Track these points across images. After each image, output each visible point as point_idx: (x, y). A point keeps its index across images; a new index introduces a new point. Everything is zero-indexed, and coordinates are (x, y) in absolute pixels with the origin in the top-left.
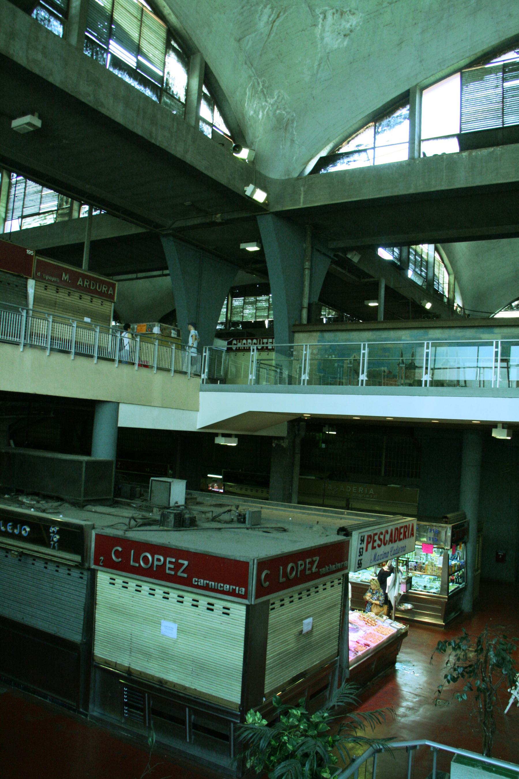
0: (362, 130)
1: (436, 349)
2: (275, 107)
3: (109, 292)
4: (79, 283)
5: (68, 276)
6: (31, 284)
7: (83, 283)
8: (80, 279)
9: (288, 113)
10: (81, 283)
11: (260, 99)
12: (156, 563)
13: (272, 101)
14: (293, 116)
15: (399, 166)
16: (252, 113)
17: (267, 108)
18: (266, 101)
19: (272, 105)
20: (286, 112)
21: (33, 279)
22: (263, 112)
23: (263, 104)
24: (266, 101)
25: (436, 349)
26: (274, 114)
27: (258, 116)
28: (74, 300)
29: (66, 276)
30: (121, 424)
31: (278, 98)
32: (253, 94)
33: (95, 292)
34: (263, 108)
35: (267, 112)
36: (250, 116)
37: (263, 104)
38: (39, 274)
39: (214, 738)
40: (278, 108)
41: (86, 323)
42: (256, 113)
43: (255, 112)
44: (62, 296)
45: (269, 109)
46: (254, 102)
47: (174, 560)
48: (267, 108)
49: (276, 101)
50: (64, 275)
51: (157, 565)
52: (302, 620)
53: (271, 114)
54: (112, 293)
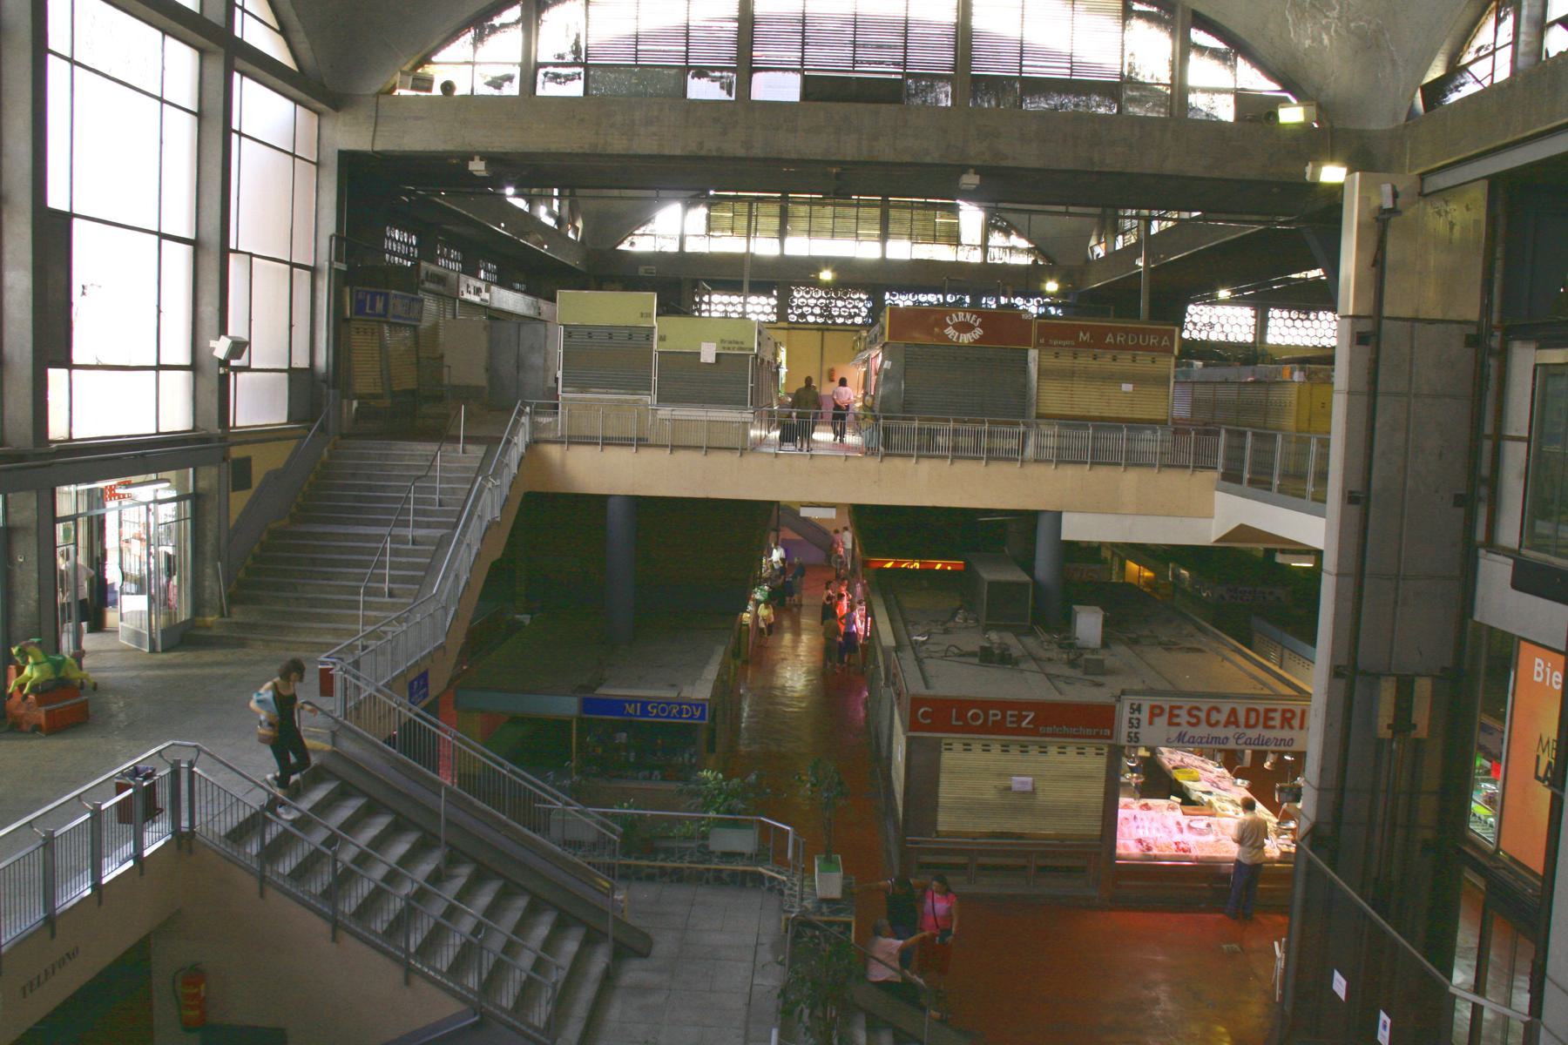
0: (1484, 18)
1: (77, 510)
2: (1344, 19)
3: (1163, 343)
4: (1108, 340)
5: (1088, 335)
6: (1033, 354)
7: (1115, 339)
8: (1110, 335)
9: (1369, 23)
10: (1112, 341)
11: (1315, 17)
12: (991, 718)
13: (1335, 14)
14: (1378, 24)
15: (676, 253)
16: (1308, 43)
17: (1333, 25)
18: (1327, 17)
19: (1339, 18)
20: (1366, 21)
21: (1034, 348)
22: (1328, 33)
23: (1324, 22)
24: (1327, 17)
25: (77, 510)
26: (1349, 31)
27: (1321, 41)
28: (1105, 362)
29: (1085, 334)
30: (1065, 537)
31: (1341, 7)
32: (1299, 16)
33: (1137, 347)
34: (1327, 28)
35: (1336, 31)
36: (1305, 49)
37: (1324, 22)
38: (1042, 341)
39: (168, 799)
40: (1349, 21)
41: (1126, 393)
42: (1317, 39)
43: (1313, 40)
44: (1084, 361)
45: (1337, 25)
46: (1305, 25)
47: (1016, 713)
48: (1333, 25)
49: (1340, 12)
50: (1081, 334)
51: (993, 721)
52: (1013, 775)
53: (1344, 33)
54: (1168, 343)
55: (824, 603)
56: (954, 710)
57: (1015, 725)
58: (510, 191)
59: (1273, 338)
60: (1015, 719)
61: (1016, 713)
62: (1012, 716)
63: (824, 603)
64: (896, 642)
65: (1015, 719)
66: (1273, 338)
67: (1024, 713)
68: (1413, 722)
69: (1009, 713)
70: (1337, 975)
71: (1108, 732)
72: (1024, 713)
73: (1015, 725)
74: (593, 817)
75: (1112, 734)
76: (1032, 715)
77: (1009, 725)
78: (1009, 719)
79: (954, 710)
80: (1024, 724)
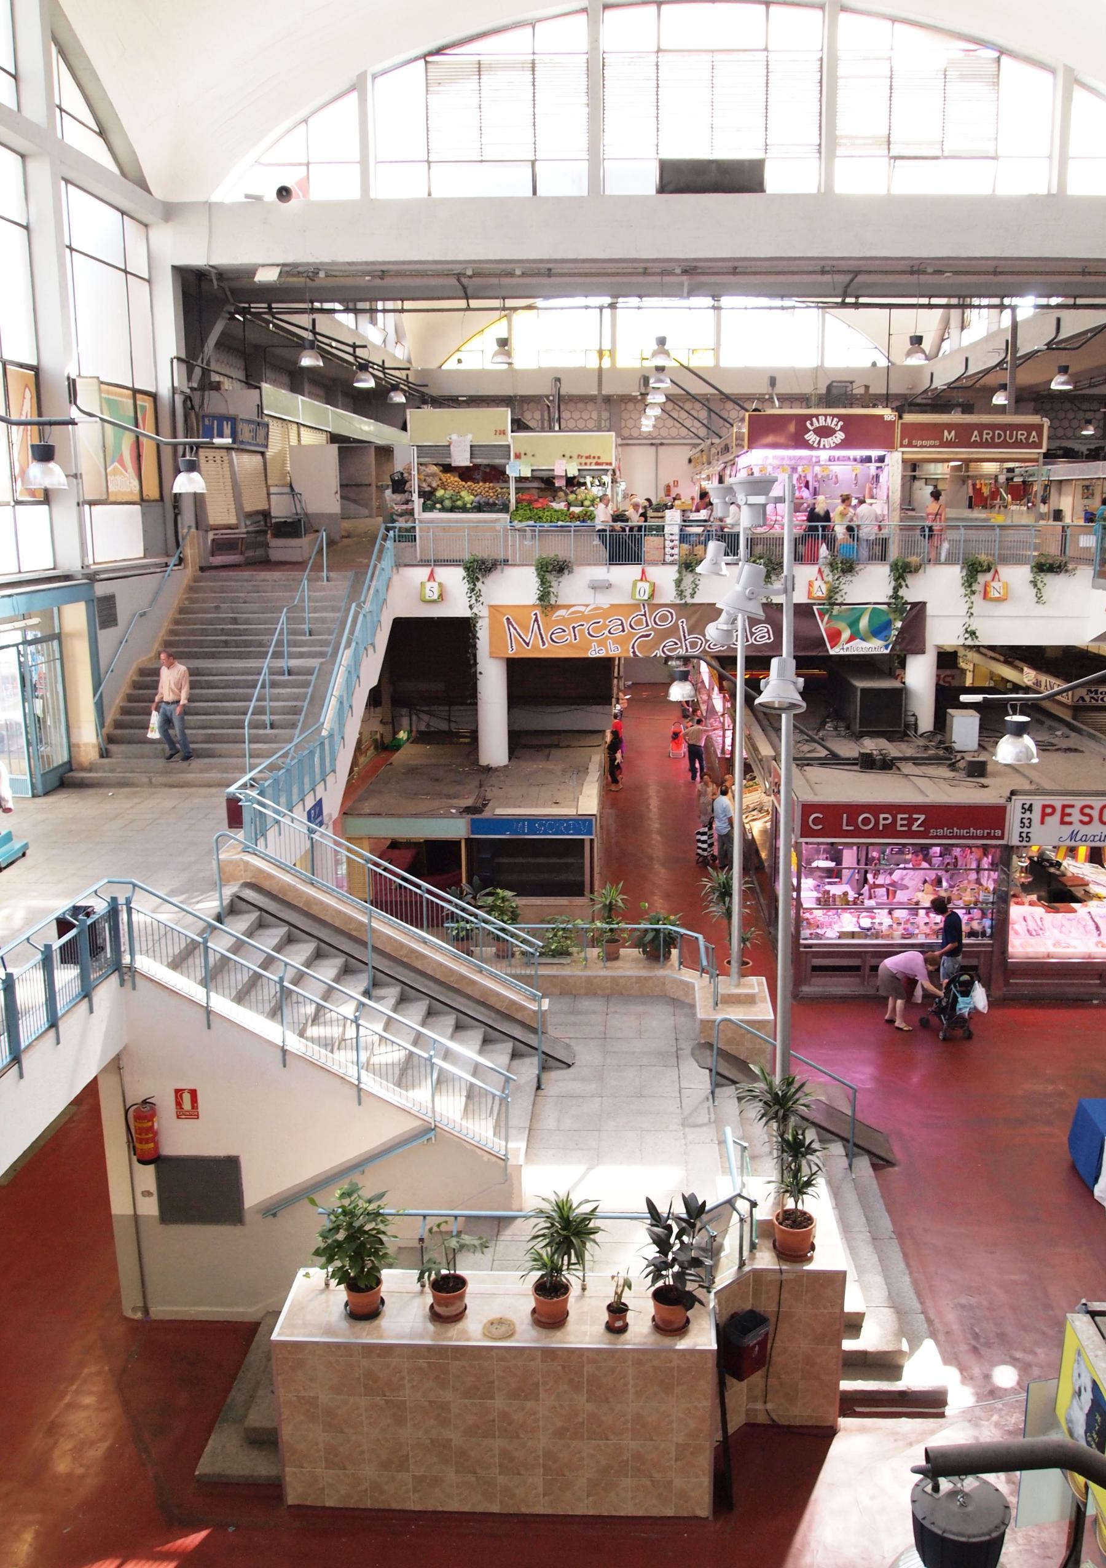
12: (882, 822)
47: (906, 816)
57: (905, 829)
61: (906, 816)
62: (902, 819)
69: (899, 816)
71: (998, 833)
73: (905, 829)
76: (922, 817)
77: (899, 828)
78: (899, 822)
80: (914, 828)
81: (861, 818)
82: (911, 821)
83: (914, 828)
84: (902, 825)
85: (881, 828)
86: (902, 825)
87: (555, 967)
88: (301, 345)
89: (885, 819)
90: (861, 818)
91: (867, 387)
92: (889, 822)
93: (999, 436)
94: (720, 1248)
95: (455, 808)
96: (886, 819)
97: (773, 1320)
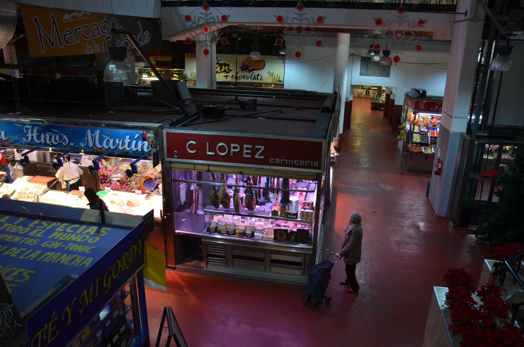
12: (233, 150)
47: (251, 146)
55: (477, 296)
56: (208, 143)
57: (250, 156)
58: (140, 22)
59: (489, 158)
60: (249, 151)
61: (251, 146)
62: (247, 149)
63: (477, 296)
64: (110, 61)
65: (249, 151)
66: (489, 158)
67: (257, 147)
68: (418, 32)
69: (245, 146)
70: (101, 331)
71: (316, 164)
72: (257, 147)
73: (250, 156)
74: (122, 265)
75: (320, 164)
76: (263, 148)
77: (245, 156)
78: (245, 151)
79: (208, 143)
80: (257, 156)
81: (221, 144)
82: (254, 151)
83: (257, 156)
84: (247, 153)
85: (232, 155)
86: (247, 153)
87: (186, 168)
88: (10, 245)
89: (234, 148)
90: (221, 144)
91: (88, 205)
92: (237, 150)
93: (297, 163)
94: (472, 130)
95: (104, 124)
96: (236, 148)
97: (222, 173)
